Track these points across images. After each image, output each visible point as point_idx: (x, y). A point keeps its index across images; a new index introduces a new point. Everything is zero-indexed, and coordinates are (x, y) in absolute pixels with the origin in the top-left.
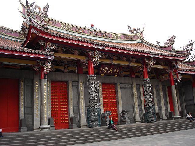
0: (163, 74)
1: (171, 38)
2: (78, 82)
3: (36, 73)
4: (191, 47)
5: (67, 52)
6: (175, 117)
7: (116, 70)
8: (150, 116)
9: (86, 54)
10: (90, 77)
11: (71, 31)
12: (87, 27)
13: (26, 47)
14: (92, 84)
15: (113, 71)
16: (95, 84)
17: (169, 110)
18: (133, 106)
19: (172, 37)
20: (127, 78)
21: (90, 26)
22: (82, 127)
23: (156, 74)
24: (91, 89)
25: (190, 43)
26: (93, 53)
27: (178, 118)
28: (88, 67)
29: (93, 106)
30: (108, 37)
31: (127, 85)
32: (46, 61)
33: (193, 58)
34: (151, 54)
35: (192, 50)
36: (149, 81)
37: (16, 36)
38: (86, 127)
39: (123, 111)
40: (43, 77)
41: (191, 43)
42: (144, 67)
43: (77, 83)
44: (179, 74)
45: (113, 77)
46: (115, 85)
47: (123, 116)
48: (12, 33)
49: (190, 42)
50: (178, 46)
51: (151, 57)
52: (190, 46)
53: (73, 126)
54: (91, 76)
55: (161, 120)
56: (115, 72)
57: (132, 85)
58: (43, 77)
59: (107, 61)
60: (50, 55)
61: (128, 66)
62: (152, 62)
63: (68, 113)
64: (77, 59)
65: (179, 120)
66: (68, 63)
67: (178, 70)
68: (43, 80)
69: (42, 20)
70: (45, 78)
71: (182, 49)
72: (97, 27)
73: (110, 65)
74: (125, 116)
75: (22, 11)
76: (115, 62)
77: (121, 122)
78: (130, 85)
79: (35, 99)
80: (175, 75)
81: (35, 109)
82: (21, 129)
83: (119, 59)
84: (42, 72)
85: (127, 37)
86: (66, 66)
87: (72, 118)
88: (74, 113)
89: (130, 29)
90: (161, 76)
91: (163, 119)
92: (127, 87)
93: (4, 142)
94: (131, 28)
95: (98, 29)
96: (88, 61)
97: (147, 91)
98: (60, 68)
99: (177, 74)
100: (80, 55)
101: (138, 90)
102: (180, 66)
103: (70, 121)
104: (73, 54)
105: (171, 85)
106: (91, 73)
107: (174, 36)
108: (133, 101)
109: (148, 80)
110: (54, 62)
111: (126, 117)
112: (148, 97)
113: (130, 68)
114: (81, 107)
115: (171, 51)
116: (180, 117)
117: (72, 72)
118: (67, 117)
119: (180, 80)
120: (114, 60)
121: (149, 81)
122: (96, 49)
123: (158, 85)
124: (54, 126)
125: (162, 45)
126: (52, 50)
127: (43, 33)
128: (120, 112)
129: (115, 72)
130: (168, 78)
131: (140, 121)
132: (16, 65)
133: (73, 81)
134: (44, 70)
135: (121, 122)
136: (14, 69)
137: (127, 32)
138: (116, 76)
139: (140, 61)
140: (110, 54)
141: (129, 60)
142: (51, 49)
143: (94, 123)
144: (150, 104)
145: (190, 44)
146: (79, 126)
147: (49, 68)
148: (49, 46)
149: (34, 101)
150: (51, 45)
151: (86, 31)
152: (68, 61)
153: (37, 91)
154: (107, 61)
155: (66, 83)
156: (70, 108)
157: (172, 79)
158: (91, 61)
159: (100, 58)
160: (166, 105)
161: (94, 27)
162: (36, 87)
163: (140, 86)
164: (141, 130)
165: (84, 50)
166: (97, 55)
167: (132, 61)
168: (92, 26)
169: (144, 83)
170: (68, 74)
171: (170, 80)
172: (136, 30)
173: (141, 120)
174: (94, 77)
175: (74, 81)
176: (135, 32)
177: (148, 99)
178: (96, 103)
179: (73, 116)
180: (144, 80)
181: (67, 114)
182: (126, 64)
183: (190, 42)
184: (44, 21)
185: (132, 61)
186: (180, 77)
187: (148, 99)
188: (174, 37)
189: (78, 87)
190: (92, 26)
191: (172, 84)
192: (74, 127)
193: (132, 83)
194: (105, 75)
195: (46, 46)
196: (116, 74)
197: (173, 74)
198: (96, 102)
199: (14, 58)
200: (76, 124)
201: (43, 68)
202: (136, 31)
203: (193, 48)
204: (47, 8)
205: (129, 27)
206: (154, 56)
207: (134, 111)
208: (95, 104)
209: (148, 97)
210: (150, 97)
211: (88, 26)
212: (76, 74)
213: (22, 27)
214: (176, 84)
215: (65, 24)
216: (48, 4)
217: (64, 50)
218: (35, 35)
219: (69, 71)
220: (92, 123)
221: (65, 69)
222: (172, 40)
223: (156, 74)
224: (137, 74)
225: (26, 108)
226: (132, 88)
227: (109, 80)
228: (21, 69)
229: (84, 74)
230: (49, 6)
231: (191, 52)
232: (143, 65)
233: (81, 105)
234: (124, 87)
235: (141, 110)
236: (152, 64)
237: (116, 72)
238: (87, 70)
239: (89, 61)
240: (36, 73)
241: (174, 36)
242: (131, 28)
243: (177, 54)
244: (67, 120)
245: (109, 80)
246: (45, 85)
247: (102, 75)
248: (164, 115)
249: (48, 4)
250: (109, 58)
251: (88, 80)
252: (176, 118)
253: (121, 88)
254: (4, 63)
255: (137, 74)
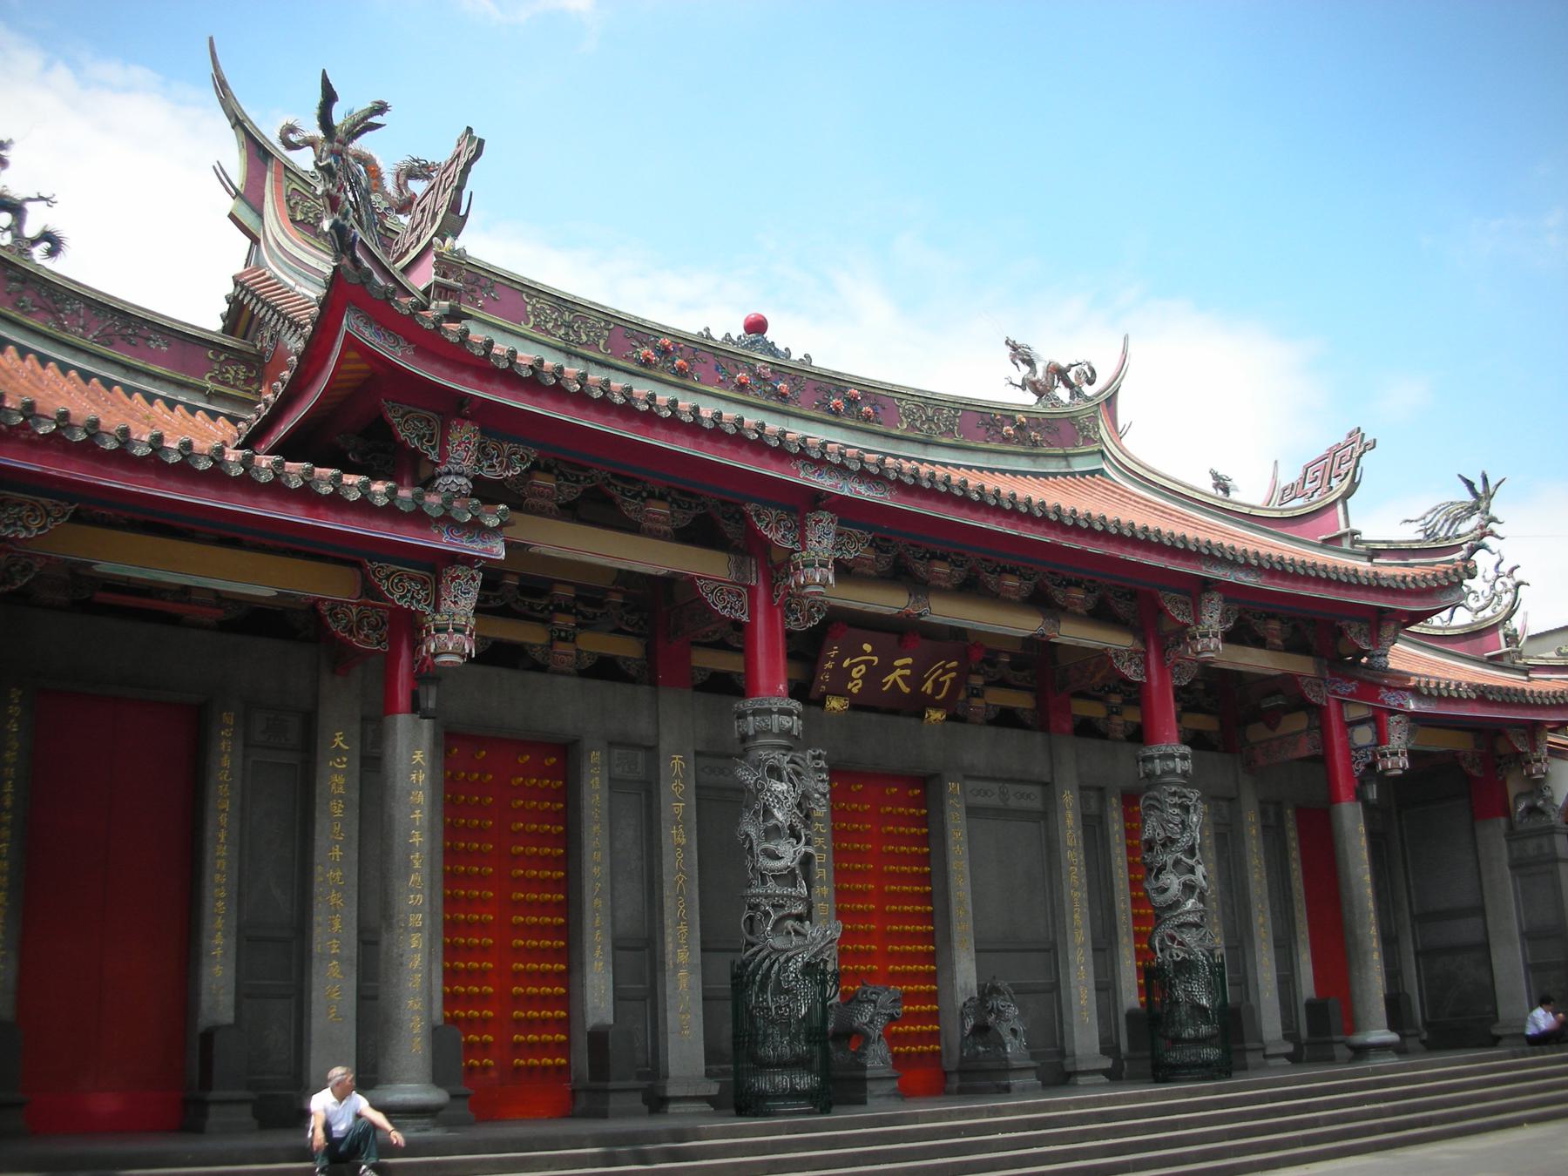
0: (1271, 718)
1: (1333, 453)
2: (652, 750)
3: (341, 657)
4: (1475, 520)
5: (594, 508)
6: (1358, 1039)
7: (943, 674)
8: (1189, 1032)
9: (730, 529)
10: (755, 713)
11: (599, 356)
12: (718, 335)
13: (288, 449)
14: (775, 772)
15: (915, 680)
16: (798, 774)
17: (1307, 987)
18: (1052, 951)
19: (1342, 439)
20: (1016, 733)
21: (738, 331)
22: (672, 1108)
23: (1227, 714)
24: (768, 814)
25: (1475, 494)
26: (789, 529)
27: (1383, 1047)
28: (736, 637)
29: (779, 942)
30: (867, 419)
31: (1012, 789)
32: (436, 565)
33: (1482, 602)
34: (1211, 557)
35: (1487, 540)
36: (1188, 765)
37: (183, 368)
38: (706, 1107)
39: (987, 992)
40: (403, 698)
41: (1479, 488)
42: (1146, 654)
43: (641, 756)
44: (1397, 718)
45: (913, 721)
46: (924, 787)
47: (982, 1030)
48: (159, 345)
49: (1470, 485)
50: (1386, 514)
51: (1207, 584)
52: (1472, 510)
53: (612, 1097)
54: (770, 712)
55: (1251, 1059)
56: (928, 687)
57: (1048, 788)
58: (403, 698)
59: (888, 602)
60: (476, 528)
61: (1030, 642)
62: (1213, 618)
63: (567, 996)
64: (663, 572)
65: (1392, 1060)
66: (578, 598)
67: (1389, 688)
68: (403, 722)
69: (413, 253)
70: (415, 707)
71: (1409, 534)
72: (791, 336)
73: (898, 633)
74: (1004, 1030)
75: (238, 179)
76: (945, 612)
77: (962, 1072)
78: (1035, 790)
79: (318, 869)
80: (1361, 722)
81: (317, 949)
82: (212, 1109)
83: (971, 588)
84: (391, 660)
85: (1008, 429)
86: (564, 621)
87: (598, 1039)
88: (619, 997)
89: (1025, 369)
90: (1257, 732)
91: (1265, 1056)
92: (1013, 803)
93: (1000, 1136)
94: (1030, 363)
95: (796, 355)
96: (750, 588)
97: (1169, 842)
98: (529, 635)
99: (1378, 720)
100: (684, 536)
101: (1093, 827)
102: (1403, 657)
103: (581, 1061)
104: (633, 528)
105: (1334, 799)
106: (763, 680)
107: (1356, 435)
108: (1056, 914)
109: (1172, 755)
110: (506, 592)
111: (1008, 1038)
112: (1173, 882)
113: (1037, 658)
114: (670, 947)
115: (1332, 542)
116: (1392, 1037)
117: (605, 669)
118: (564, 1025)
119: (1403, 762)
120: (941, 592)
121: (1188, 765)
122: (816, 500)
123: (1231, 800)
124: (1032, 1064)
125: (1251, 492)
126: (485, 491)
127: (431, 345)
128: (961, 999)
129: (928, 687)
130: (1306, 748)
131: (1105, 1072)
132: (186, 589)
133: (611, 744)
134: (416, 644)
135: (962, 1072)
136: (173, 620)
137: (994, 383)
138: (936, 715)
139: (1121, 608)
140: (921, 539)
141: (1038, 601)
142: (476, 480)
143: (783, 1081)
144: (1189, 937)
145: (1470, 498)
146: (657, 1103)
147: (454, 629)
148: (461, 459)
149: (318, 889)
150: (482, 449)
151: (712, 361)
152: (577, 586)
153: (337, 809)
154: (888, 602)
155: (564, 755)
156: (588, 958)
157: (1338, 752)
158: (771, 587)
159: (844, 571)
160: (1284, 948)
161: (770, 335)
162: (337, 780)
163: (1103, 800)
164: (1331, 1102)
165: (726, 500)
166: (818, 564)
167: (1064, 609)
168: (757, 326)
169: (1150, 775)
170: (574, 682)
171: (1323, 759)
172: (1071, 375)
173: (1107, 1063)
174: (786, 722)
175: (620, 745)
176: (1063, 393)
177: (1176, 904)
178: (797, 925)
179: (610, 1020)
180: (1151, 759)
181: (563, 1001)
182: (1025, 624)
183: (1470, 485)
184: (432, 258)
185: (1064, 609)
186: (1398, 739)
187: (1176, 904)
188: (1358, 444)
189: (648, 792)
190: (757, 326)
191: (1343, 791)
192: (615, 1102)
193: (1047, 779)
194: (857, 706)
195: (443, 455)
196: (937, 706)
197: (1353, 713)
198: (799, 918)
199: (234, 543)
200: (632, 1083)
201: (408, 627)
202: (1068, 384)
203: (1492, 526)
204: (463, 160)
205: (1021, 355)
206: (1233, 577)
207: (1053, 990)
208: (797, 933)
209: (1173, 882)
210: (1189, 888)
211: (726, 325)
212: (643, 691)
213: (233, 300)
214: (1372, 793)
215: (562, 303)
216: (469, 130)
217: (571, 492)
218: (383, 360)
219: (588, 663)
220: (763, 1084)
221: (561, 647)
222: (1342, 466)
223: (1227, 714)
224: (1083, 708)
225: (248, 940)
226: (1046, 816)
227: (890, 743)
228: (225, 627)
229: (697, 688)
230: (481, 143)
231: (1480, 557)
232: (1145, 642)
233: (668, 931)
234: (994, 801)
235: (1106, 987)
236: (818, 564)
237: (938, 686)
238: (728, 663)
239: (752, 591)
240: (341, 657)
241: (1356, 435)
242: (1030, 363)
243: (1389, 569)
244: (563, 1048)
245: (890, 743)
246: (413, 756)
247: (835, 704)
248: (1271, 1025)
249: (469, 130)
250: (899, 575)
251: (744, 738)
252: (1361, 1052)
253: (972, 811)
254: (105, 567)
255: (1083, 708)
